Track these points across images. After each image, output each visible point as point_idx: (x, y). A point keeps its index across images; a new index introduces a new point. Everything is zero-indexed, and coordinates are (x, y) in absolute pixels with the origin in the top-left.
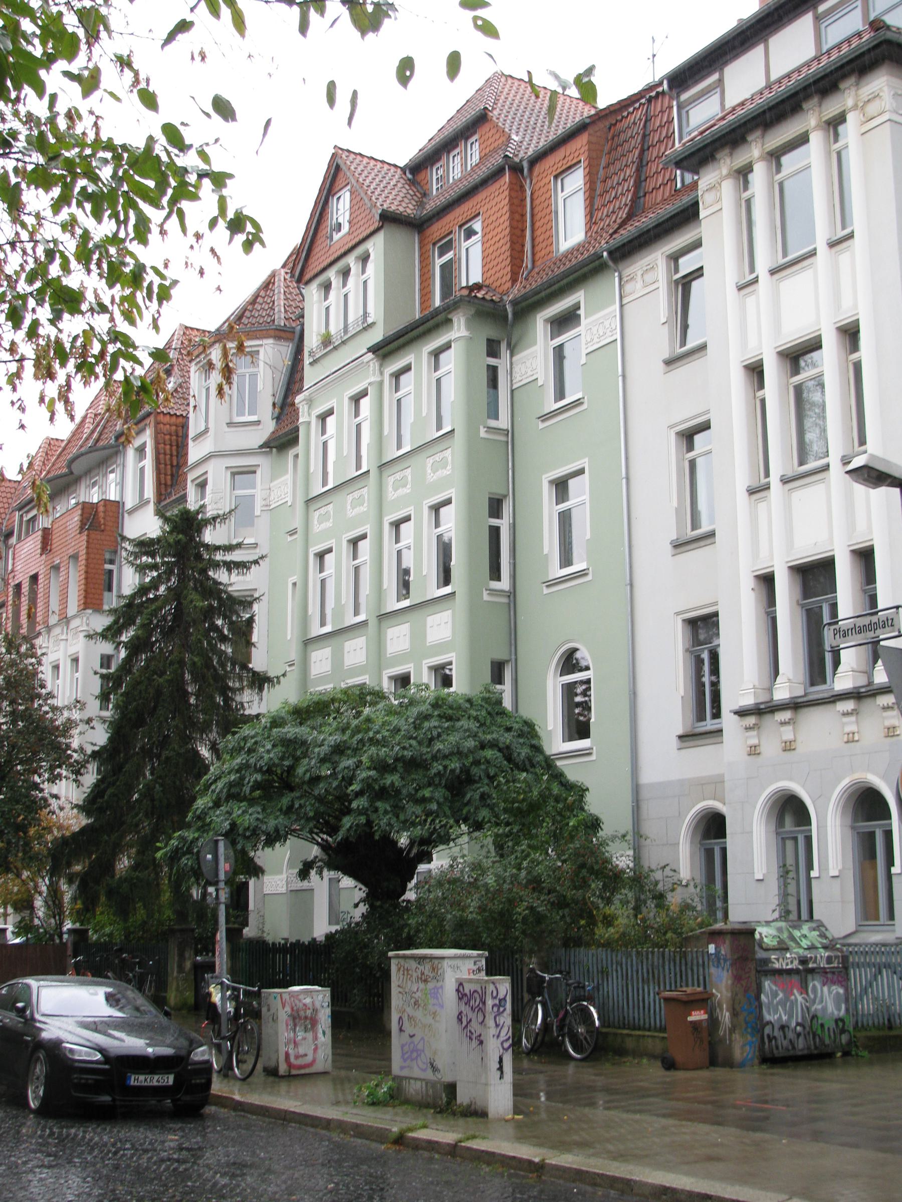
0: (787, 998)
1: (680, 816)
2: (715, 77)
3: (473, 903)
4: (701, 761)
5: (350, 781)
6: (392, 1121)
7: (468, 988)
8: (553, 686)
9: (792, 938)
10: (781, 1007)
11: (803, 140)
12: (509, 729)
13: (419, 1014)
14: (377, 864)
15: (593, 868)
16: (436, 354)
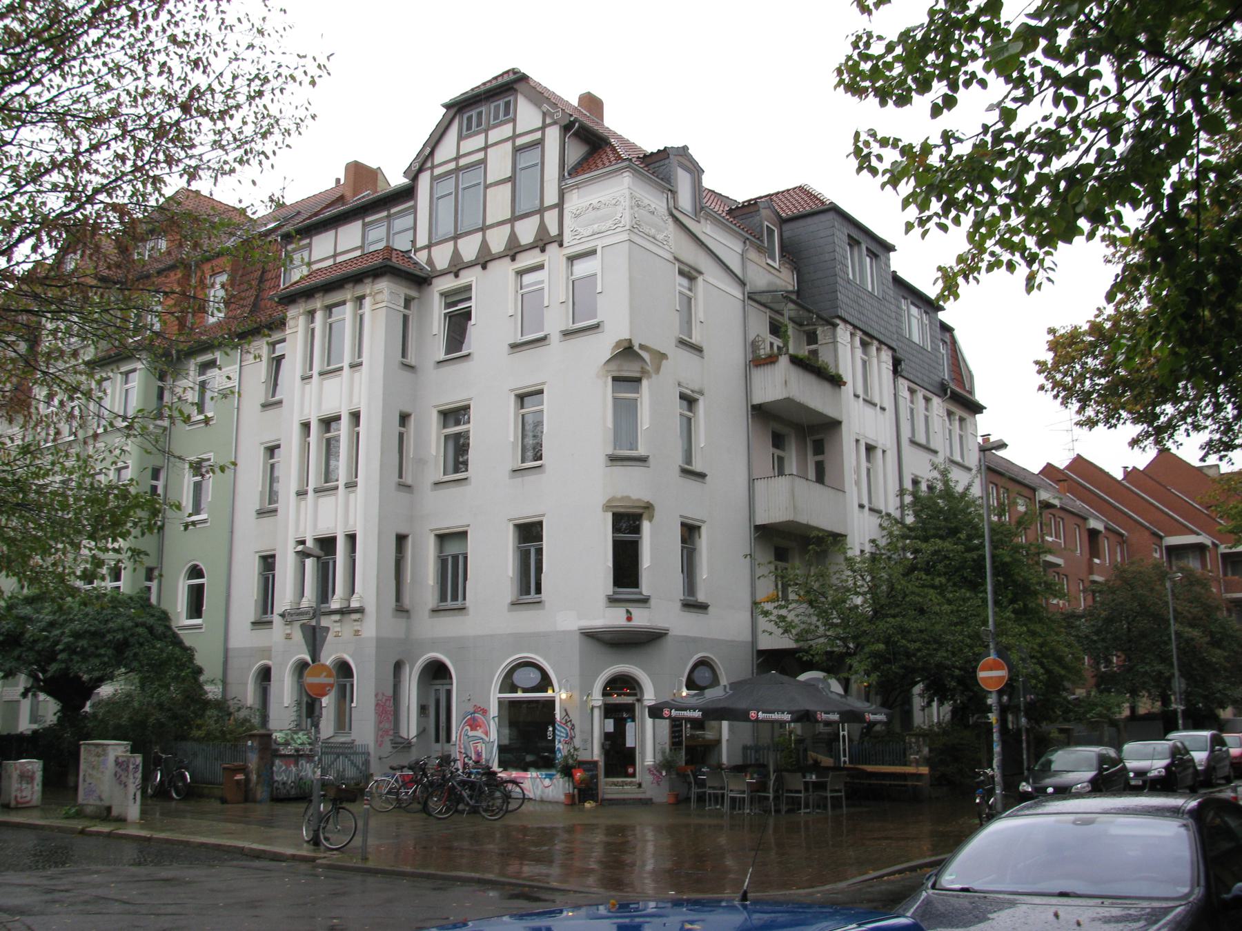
1: (250, 668)
2: (308, 241)
3: (126, 716)
4: (261, 638)
5: (57, 643)
6: (79, 825)
7: (121, 760)
8: (182, 586)
9: (292, 739)
10: (283, 773)
11: (344, 303)
12: (153, 616)
13: (94, 772)
14: (70, 691)
15: (195, 699)
16: (127, 374)
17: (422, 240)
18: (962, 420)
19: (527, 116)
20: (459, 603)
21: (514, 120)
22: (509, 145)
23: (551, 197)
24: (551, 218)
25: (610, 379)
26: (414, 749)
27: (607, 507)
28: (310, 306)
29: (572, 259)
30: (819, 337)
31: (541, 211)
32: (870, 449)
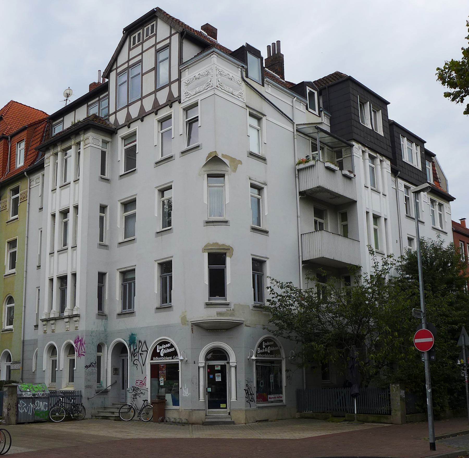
0: (27, 405)
2: (62, 119)
17: (112, 110)
18: (440, 205)
19: (163, 30)
20: (131, 310)
21: (156, 35)
22: (153, 49)
23: (175, 76)
24: (175, 87)
25: (206, 176)
26: (110, 394)
27: (204, 250)
28: (55, 151)
29: (186, 110)
30: (343, 154)
31: (170, 84)
32: (376, 218)
